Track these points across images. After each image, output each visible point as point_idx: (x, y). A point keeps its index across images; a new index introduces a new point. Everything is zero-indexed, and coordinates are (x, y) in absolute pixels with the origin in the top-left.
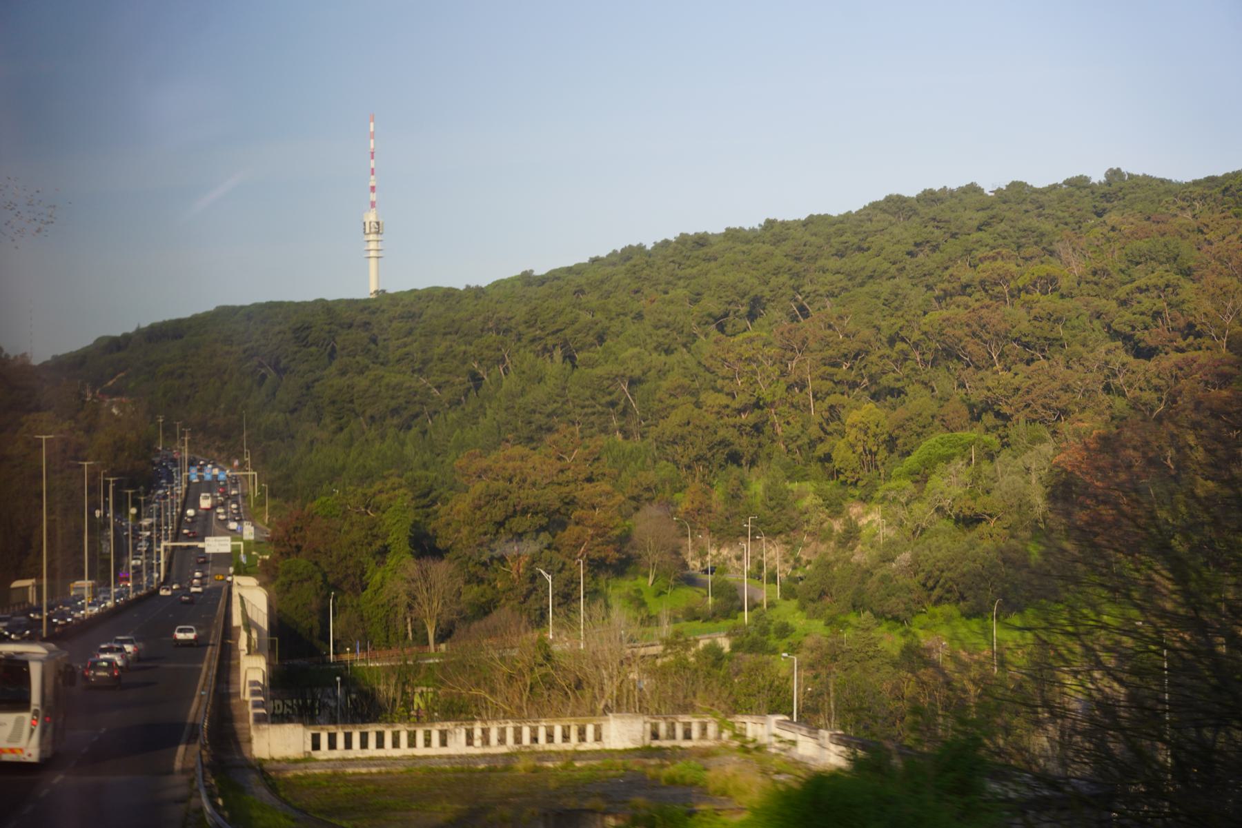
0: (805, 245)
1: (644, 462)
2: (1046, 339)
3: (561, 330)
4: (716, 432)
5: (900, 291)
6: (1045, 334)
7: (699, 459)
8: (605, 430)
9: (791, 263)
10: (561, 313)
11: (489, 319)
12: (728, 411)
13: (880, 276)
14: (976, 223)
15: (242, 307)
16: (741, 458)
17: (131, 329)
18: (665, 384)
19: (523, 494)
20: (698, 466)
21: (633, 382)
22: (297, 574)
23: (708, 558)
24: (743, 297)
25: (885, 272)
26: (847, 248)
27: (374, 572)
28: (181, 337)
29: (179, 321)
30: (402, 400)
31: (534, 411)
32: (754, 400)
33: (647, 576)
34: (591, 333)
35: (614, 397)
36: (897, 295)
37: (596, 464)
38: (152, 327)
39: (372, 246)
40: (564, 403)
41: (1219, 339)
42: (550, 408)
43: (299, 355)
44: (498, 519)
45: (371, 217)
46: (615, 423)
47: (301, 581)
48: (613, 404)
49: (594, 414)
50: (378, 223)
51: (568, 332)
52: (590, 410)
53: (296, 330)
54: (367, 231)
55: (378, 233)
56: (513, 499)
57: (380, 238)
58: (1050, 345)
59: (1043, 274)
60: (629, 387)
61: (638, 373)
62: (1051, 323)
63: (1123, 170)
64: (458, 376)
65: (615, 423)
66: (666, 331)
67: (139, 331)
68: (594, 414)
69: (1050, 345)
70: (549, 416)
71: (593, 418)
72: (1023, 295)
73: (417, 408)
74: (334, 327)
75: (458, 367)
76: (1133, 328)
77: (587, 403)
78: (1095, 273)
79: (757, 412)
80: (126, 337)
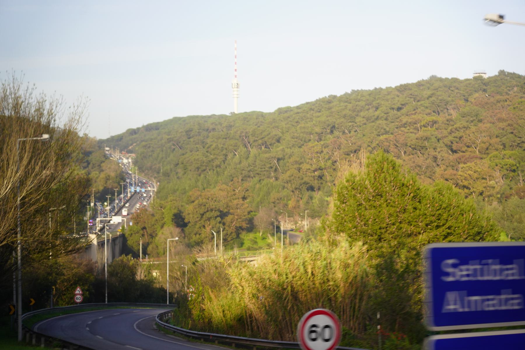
0: (357, 106)
1: (278, 190)
2: (420, 146)
3: (264, 138)
4: (302, 179)
5: (380, 126)
6: (420, 145)
7: (296, 189)
8: (268, 177)
9: (350, 113)
10: (264, 131)
11: (242, 132)
12: (309, 171)
13: (381, 119)
14: (427, 96)
15: (183, 118)
16: (315, 188)
17: (140, 126)
18: (291, 160)
19: (211, 204)
20: (296, 191)
21: (279, 160)
22: (134, 231)
23: (298, 225)
24: (328, 127)
25: (382, 117)
26: (379, 105)
27: (159, 231)
28: (158, 129)
29: (158, 123)
30: (199, 165)
31: (243, 170)
32: (319, 167)
33: (260, 232)
34: (274, 139)
35: (272, 165)
36: (379, 127)
37: (247, 192)
38: (148, 125)
39: (235, 93)
40: (254, 167)
41: (476, 148)
42: (249, 169)
43: (186, 141)
44: (202, 213)
45: (235, 81)
46: (273, 174)
47: (135, 234)
48: (271, 168)
49: (265, 171)
50: (237, 84)
51: (266, 139)
52: (264, 170)
53: (187, 132)
54: (233, 87)
55: (237, 88)
56: (207, 206)
57: (238, 89)
58: (422, 149)
59: (431, 120)
60: (277, 161)
61: (280, 156)
62: (422, 141)
63: (505, 70)
64: (220, 156)
65: (273, 174)
66: (296, 140)
67: (143, 127)
68: (265, 171)
69: (422, 149)
70: (249, 171)
71: (265, 172)
72: (423, 128)
73: (204, 168)
74: (201, 131)
75: (220, 153)
76: (452, 143)
77: (263, 167)
78: (447, 121)
79: (320, 171)
80: (138, 129)
